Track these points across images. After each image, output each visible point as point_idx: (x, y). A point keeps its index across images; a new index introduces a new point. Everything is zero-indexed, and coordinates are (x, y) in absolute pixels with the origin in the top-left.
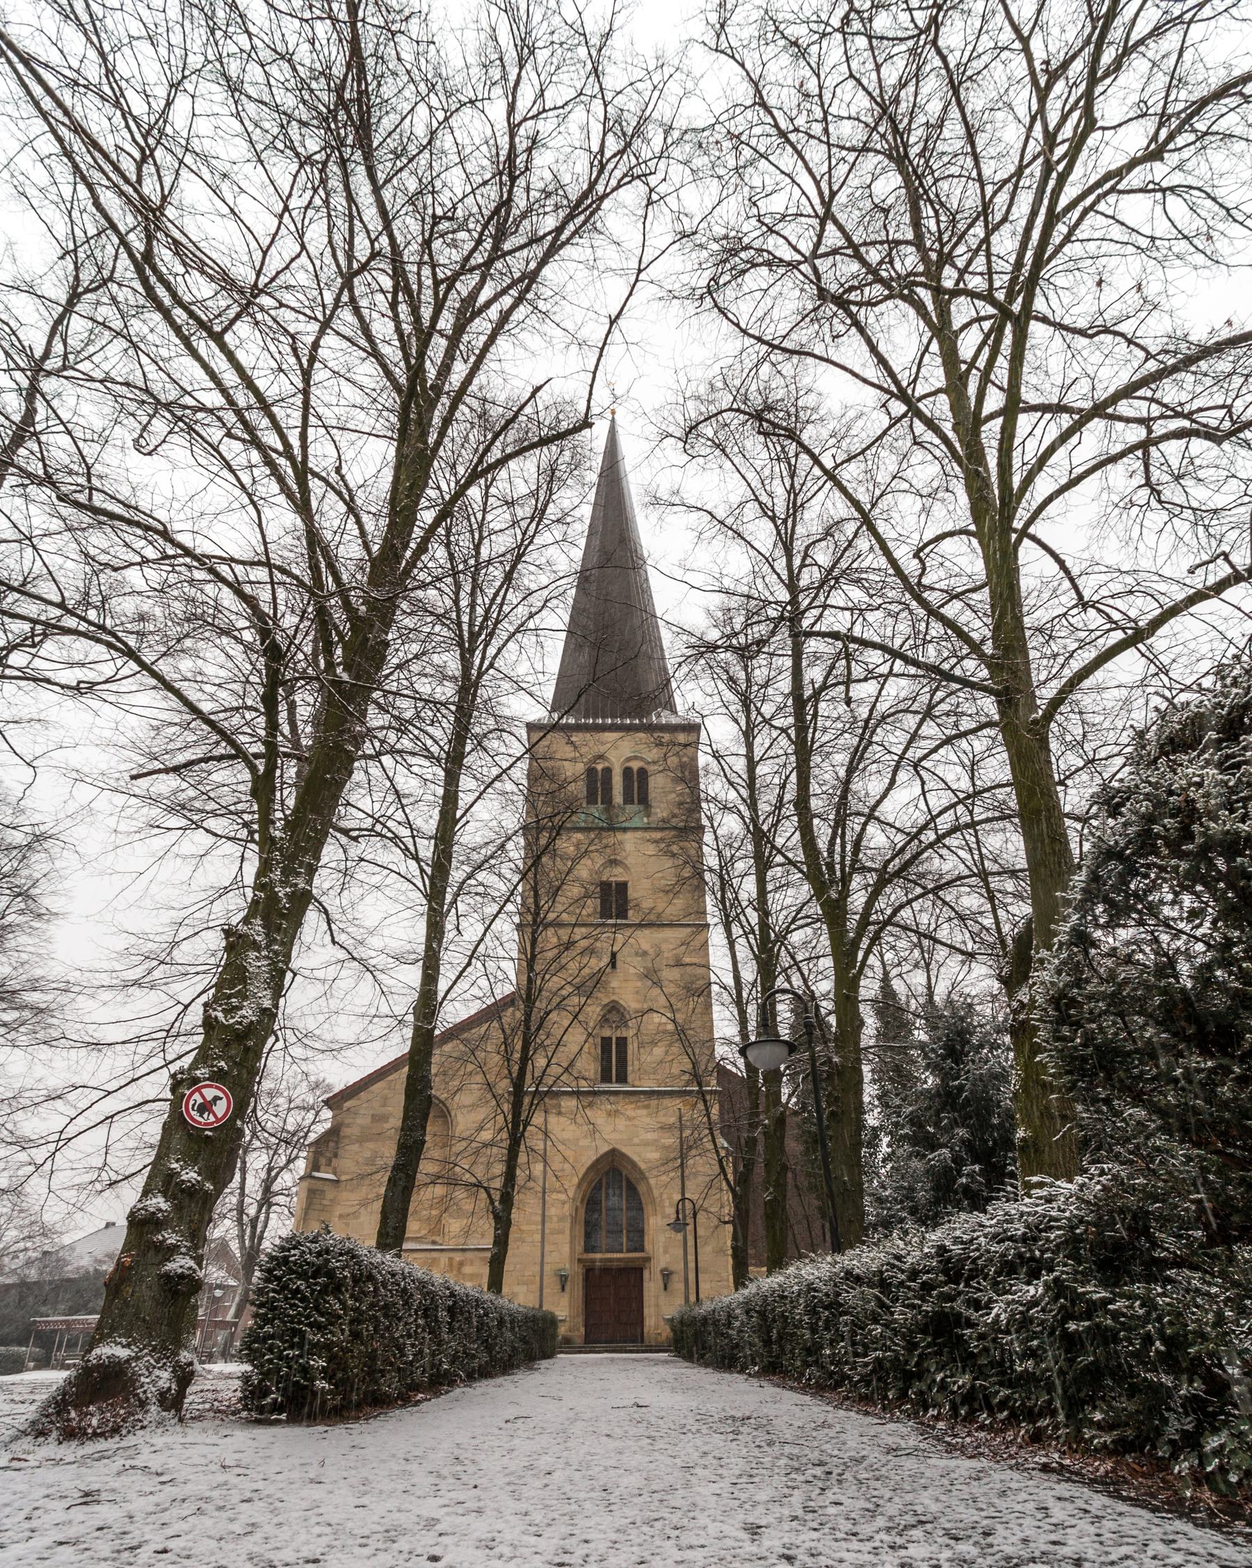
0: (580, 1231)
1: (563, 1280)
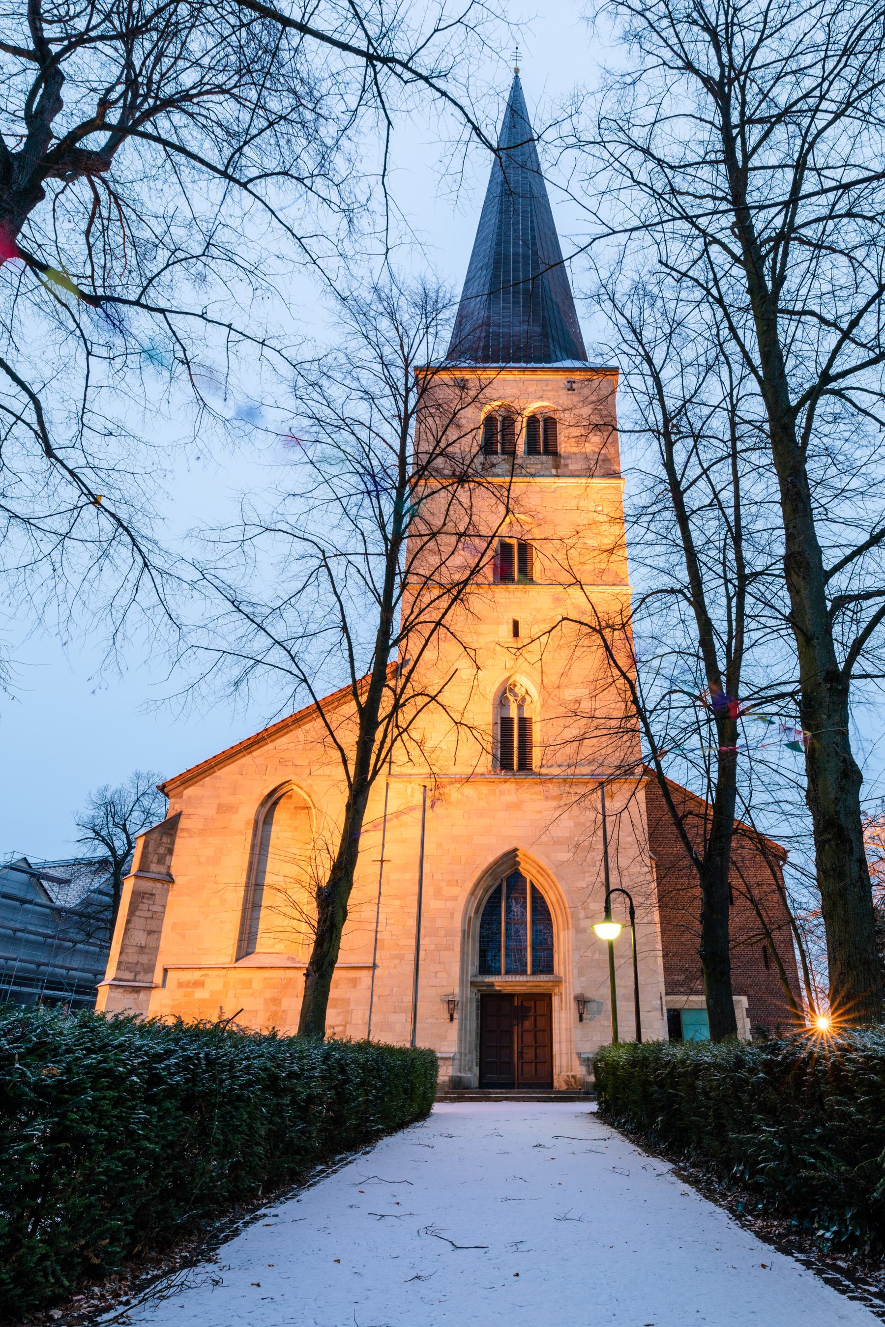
0: (474, 948)
1: (451, 1005)
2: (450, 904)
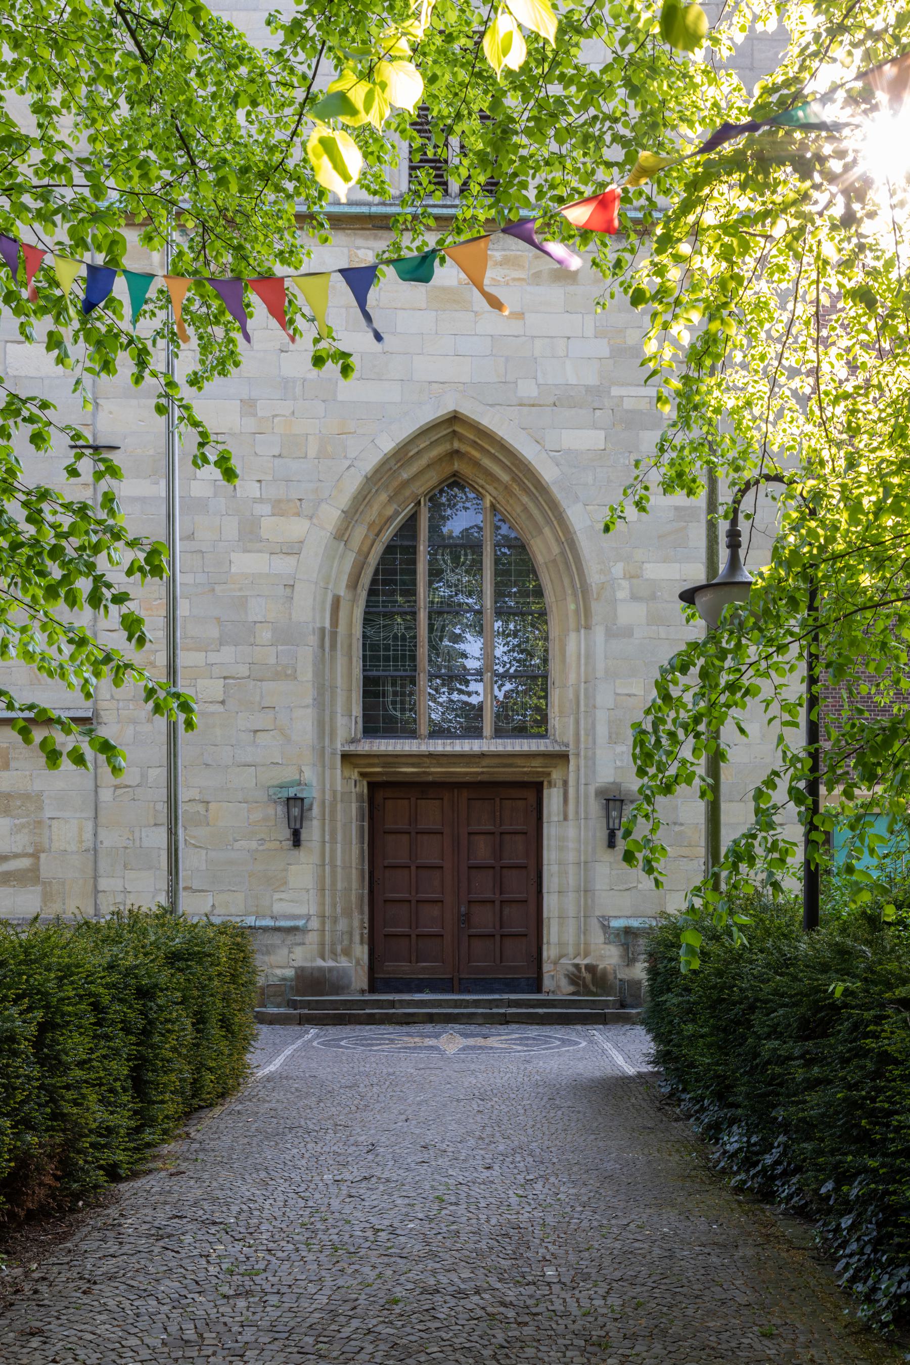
2: (283, 565)
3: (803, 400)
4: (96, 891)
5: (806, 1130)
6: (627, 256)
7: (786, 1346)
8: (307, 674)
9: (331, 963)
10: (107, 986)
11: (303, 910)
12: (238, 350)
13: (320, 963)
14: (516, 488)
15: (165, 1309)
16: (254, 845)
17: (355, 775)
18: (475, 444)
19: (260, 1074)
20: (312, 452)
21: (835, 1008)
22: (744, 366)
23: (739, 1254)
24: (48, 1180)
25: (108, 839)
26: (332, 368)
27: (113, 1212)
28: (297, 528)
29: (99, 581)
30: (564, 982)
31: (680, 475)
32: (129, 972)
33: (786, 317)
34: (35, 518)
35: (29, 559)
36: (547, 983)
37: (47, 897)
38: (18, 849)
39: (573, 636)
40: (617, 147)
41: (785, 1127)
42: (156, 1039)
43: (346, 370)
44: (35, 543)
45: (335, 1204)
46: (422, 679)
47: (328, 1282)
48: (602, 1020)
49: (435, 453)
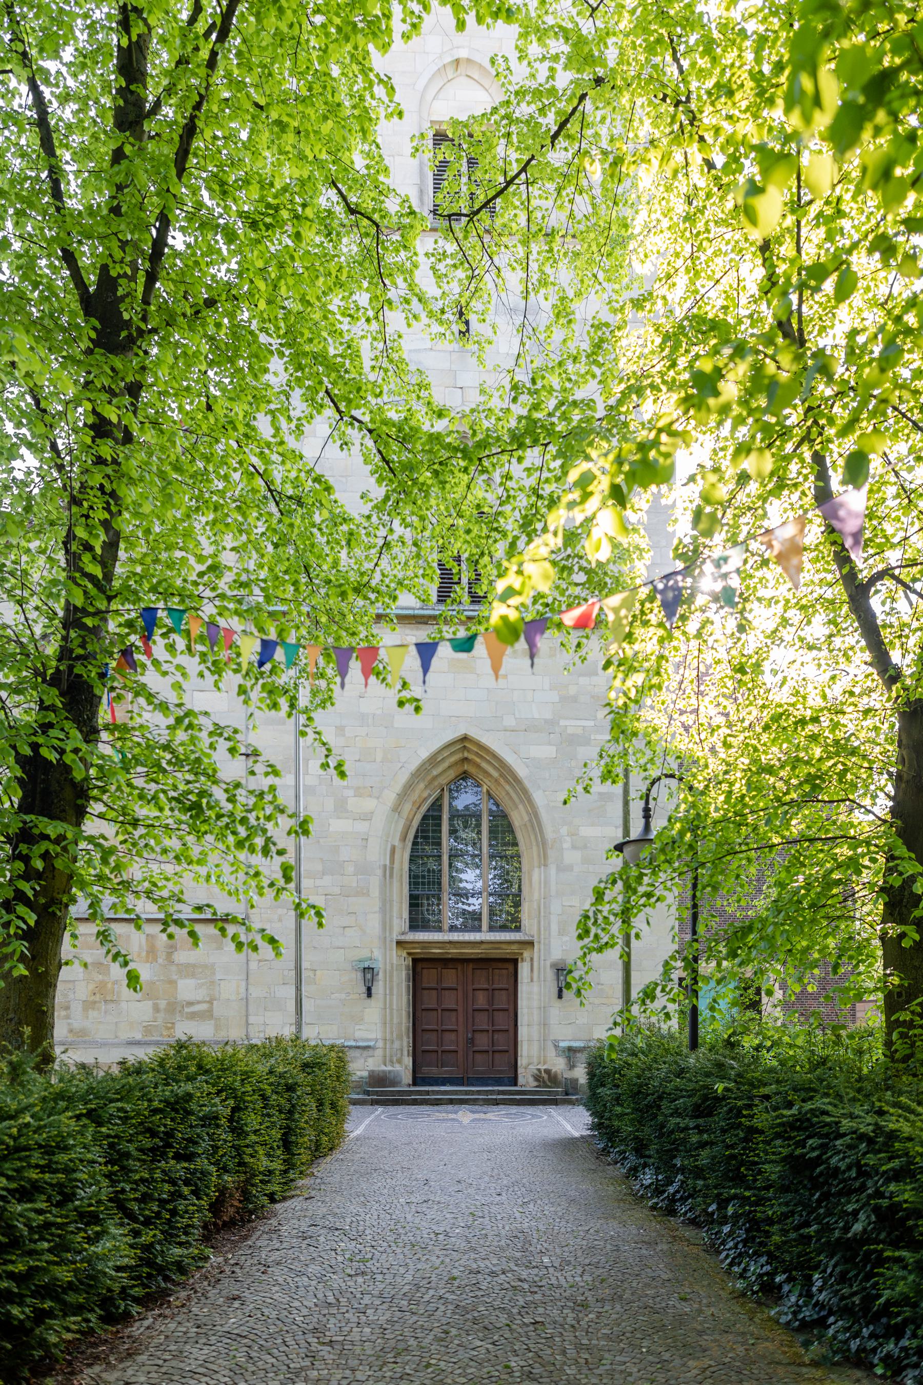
2: (362, 827)
3: (687, 729)
4: (248, 1024)
5: (698, 1173)
6: (584, 641)
7: (696, 1306)
8: (375, 892)
9: (389, 1068)
10: (271, 1084)
11: (373, 1036)
12: (334, 695)
13: (383, 1068)
14: (502, 781)
15: (314, 1283)
16: (343, 996)
17: (404, 954)
18: (477, 754)
19: (352, 1135)
20: (379, 759)
21: (718, 1099)
22: (652, 708)
23: (659, 1248)
24: (236, 1203)
25: (255, 992)
26: (409, 708)
27: (273, 1221)
28: (369, 804)
29: (268, 840)
30: (531, 1080)
31: (609, 772)
32: (281, 1076)
33: (678, 678)
34: (232, 800)
35: (227, 826)
36: (521, 1080)
37: (217, 1027)
38: (199, 998)
39: (536, 870)
40: (582, 574)
41: (682, 1170)
42: (297, 1116)
43: (417, 709)
44: (231, 815)
45: (409, 1217)
46: (445, 896)
47: (411, 1267)
48: (555, 1102)
49: (453, 759)
